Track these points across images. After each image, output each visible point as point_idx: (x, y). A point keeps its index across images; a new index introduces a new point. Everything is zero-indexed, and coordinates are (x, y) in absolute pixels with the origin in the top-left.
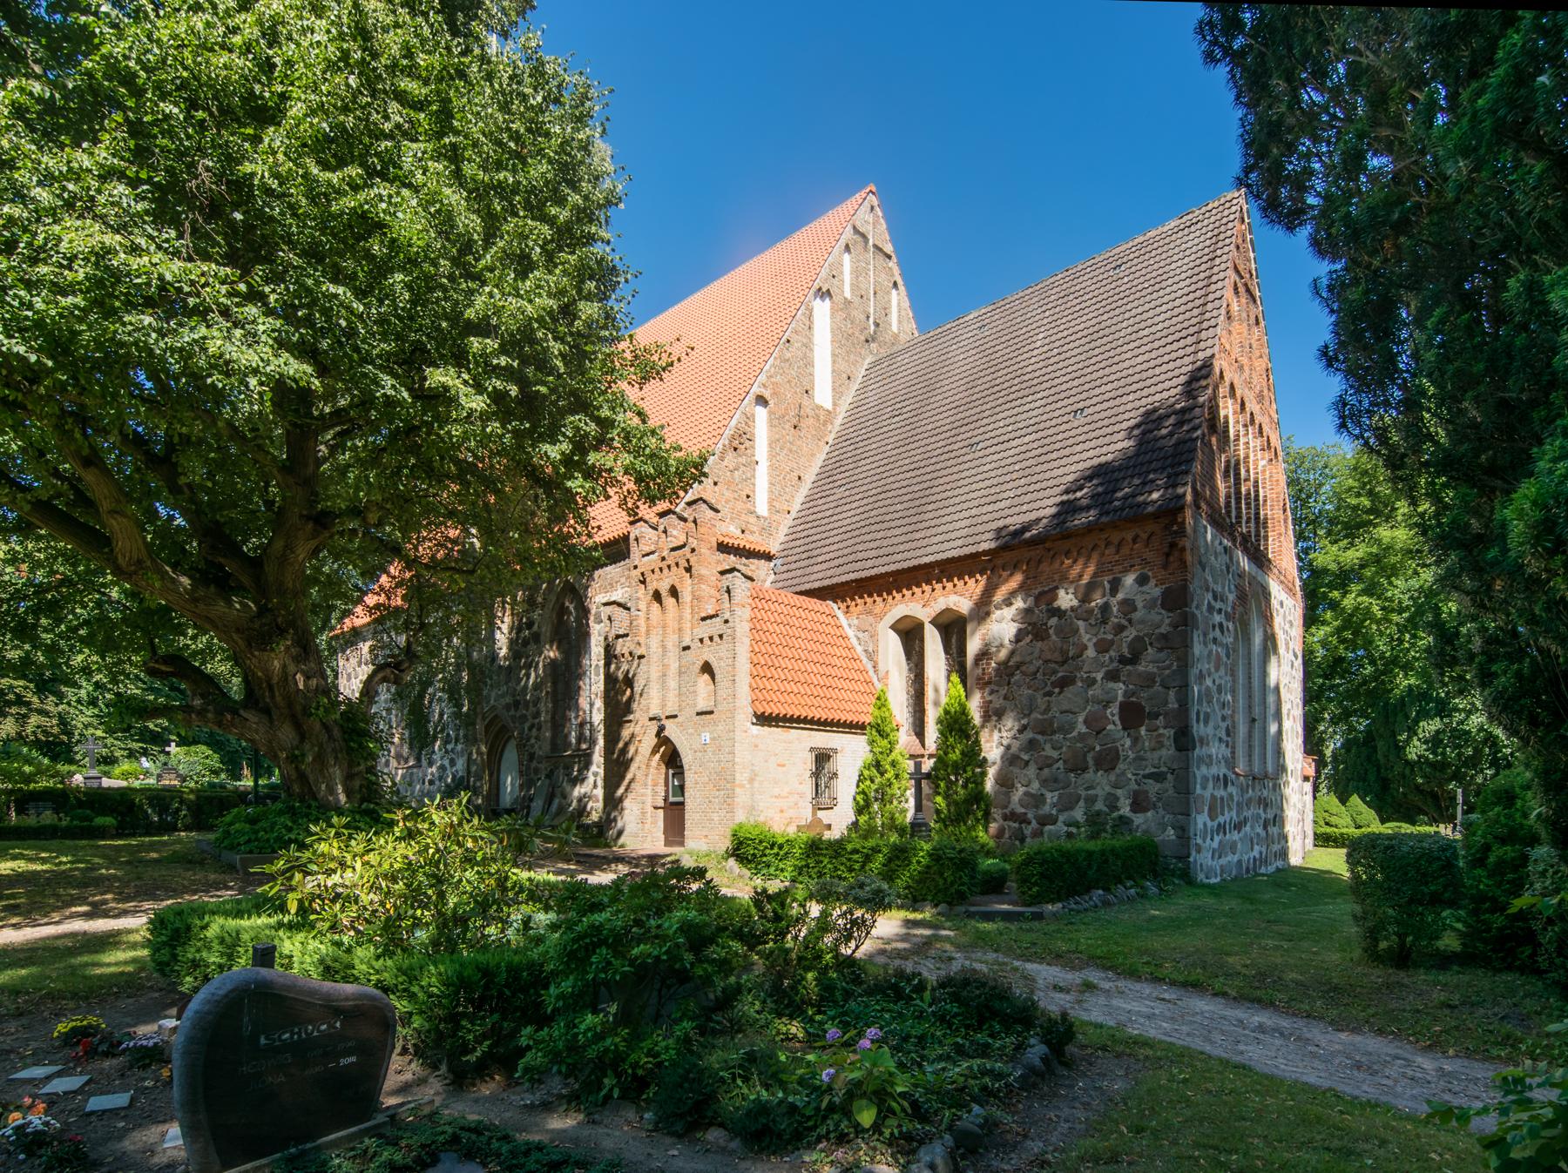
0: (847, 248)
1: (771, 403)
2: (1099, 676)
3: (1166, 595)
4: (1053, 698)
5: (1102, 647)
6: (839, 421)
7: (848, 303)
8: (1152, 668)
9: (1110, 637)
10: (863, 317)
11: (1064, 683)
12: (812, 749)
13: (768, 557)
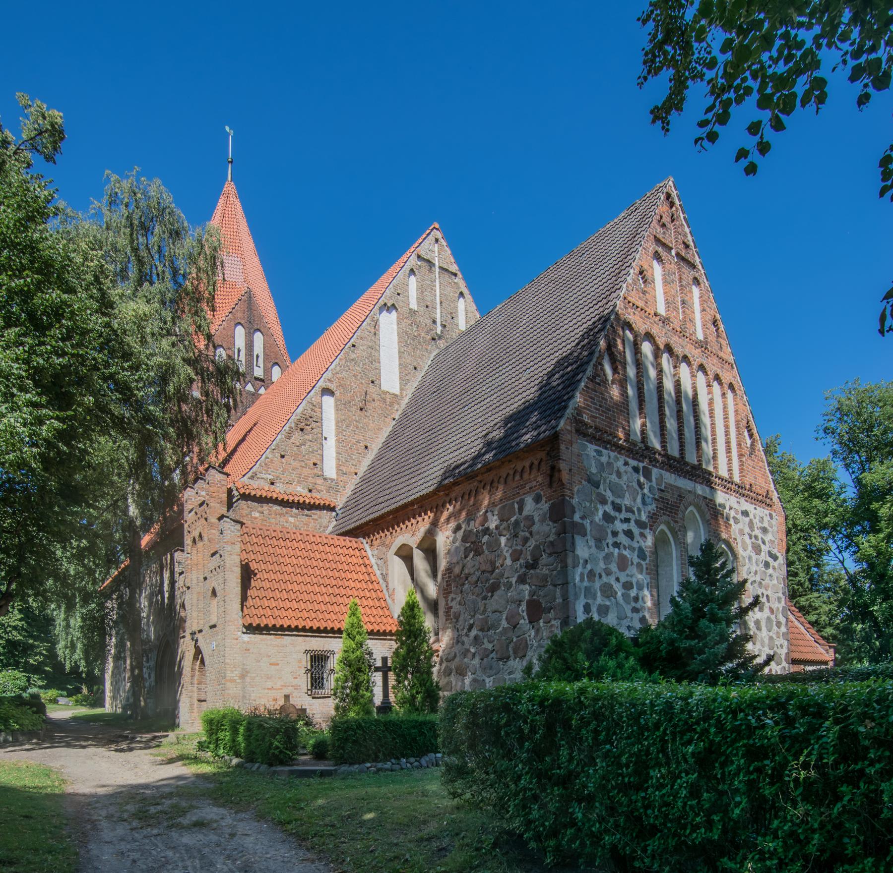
0: (412, 272)
1: (337, 393)
2: (514, 580)
3: (552, 508)
4: (487, 601)
5: (516, 557)
6: (406, 400)
7: (412, 312)
8: (545, 571)
9: (519, 548)
10: (429, 322)
11: (494, 588)
12: (307, 652)
13: (333, 509)
